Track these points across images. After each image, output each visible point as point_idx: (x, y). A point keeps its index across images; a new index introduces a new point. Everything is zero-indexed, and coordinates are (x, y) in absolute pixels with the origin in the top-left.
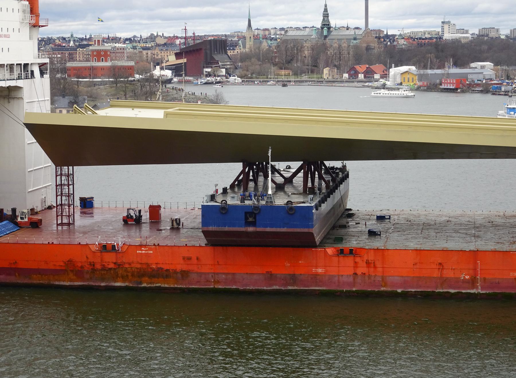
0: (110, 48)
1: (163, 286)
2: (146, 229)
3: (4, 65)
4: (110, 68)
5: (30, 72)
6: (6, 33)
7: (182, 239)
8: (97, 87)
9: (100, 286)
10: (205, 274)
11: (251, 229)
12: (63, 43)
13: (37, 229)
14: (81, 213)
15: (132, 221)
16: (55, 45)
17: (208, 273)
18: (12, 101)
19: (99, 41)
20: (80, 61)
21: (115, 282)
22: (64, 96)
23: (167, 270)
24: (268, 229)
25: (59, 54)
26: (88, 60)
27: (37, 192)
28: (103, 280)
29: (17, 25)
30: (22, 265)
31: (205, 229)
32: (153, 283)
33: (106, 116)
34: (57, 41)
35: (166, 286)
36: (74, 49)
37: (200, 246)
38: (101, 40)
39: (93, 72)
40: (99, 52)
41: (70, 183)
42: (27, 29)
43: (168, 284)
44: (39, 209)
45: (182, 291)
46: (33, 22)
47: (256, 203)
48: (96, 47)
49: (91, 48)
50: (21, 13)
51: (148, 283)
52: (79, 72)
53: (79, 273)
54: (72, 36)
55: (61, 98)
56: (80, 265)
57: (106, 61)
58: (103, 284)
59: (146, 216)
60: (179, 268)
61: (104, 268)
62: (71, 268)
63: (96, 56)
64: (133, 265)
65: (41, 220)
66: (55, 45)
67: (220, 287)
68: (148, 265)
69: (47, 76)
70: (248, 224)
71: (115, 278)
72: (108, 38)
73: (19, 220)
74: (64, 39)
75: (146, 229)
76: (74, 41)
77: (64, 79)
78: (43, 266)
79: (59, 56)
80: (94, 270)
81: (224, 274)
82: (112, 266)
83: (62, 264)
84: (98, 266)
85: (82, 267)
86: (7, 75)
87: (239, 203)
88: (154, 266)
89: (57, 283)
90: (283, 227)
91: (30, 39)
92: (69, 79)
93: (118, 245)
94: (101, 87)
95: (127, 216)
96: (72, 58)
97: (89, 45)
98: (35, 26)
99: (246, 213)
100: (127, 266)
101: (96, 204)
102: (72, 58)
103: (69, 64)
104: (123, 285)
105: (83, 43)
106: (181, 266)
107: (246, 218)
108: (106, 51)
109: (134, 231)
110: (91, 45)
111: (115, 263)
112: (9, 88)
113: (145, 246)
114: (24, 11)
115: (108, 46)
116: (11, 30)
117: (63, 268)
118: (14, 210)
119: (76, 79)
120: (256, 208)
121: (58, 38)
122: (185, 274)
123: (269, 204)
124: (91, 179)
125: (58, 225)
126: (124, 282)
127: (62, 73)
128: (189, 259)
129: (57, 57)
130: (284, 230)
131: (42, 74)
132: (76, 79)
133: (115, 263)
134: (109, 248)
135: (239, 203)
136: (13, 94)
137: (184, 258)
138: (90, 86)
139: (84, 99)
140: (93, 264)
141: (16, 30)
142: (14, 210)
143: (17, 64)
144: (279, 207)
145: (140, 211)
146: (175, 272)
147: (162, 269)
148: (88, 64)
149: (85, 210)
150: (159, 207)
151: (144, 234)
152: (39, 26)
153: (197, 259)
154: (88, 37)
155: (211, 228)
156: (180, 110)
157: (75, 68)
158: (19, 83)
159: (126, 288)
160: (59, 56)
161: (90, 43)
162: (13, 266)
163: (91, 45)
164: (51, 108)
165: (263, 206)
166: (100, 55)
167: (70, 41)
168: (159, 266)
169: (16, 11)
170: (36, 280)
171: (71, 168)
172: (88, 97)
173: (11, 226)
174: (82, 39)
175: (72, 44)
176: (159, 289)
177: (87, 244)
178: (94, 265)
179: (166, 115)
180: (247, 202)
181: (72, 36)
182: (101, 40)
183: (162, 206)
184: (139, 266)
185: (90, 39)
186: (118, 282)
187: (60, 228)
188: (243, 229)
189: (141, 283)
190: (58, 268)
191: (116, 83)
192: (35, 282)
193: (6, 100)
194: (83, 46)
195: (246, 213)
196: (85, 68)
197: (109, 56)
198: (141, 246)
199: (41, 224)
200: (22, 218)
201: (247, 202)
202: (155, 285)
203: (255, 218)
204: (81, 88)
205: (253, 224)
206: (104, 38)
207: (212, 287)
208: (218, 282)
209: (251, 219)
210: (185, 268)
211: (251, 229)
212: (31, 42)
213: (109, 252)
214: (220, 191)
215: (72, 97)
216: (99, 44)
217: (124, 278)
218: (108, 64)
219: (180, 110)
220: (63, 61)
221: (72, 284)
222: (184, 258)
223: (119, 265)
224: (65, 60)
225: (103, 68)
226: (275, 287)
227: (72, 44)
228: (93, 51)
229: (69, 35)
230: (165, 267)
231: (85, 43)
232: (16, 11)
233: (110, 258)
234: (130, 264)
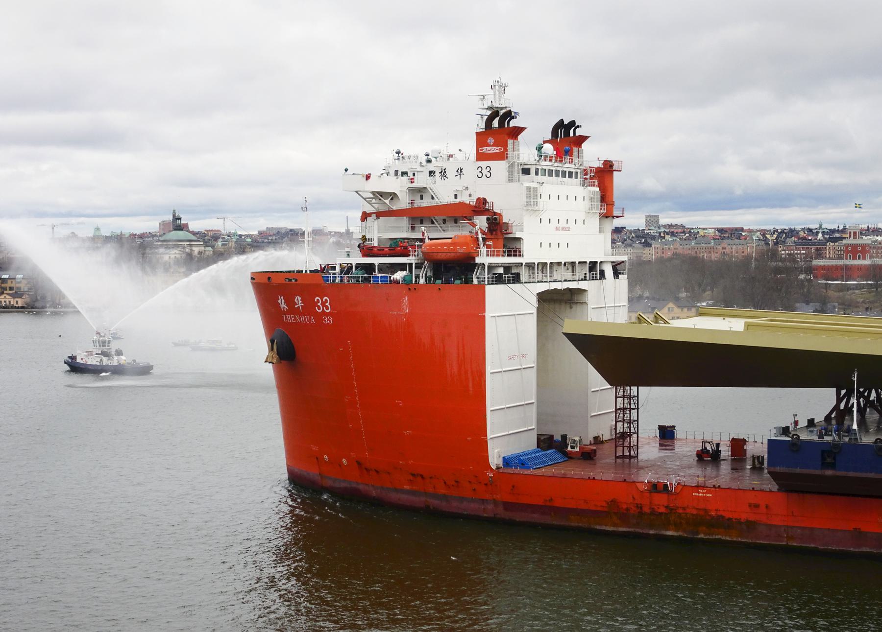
0: (870, 242)
1: (724, 538)
2: (725, 467)
3: (585, 262)
4: (867, 268)
5: (598, 272)
6: (565, 225)
7: (748, 480)
8: (850, 292)
9: (649, 534)
10: (775, 526)
11: (829, 472)
12: (808, 235)
13: (591, 462)
14: (661, 445)
15: (708, 456)
16: (799, 238)
17: (780, 526)
18: (574, 307)
19: (855, 233)
20: (830, 258)
21: (667, 530)
22: (807, 303)
23: (729, 519)
24: (851, 474)
25: (803, 249)
26: (840, 258)
27: (606, 416)
28: (651, 527)
29: (581, 216)
30: (558, 503)
31: (772, 469)
32: (712, 534)
33: (730, 331)
34: (802, 233)
35: (728, 539)
36: (823, 243)
37: (771, 491)
38: (858, 231)
39: (846, 272)
40: (854, 246)
41: (633, 406)
42: (596, 220)
43: (730, 536)
44: (605, 438)
45: (747, 546)
46: (604, 211)
47: (836, 438)
48: (851, 241)
49: (844, 242)
50: (587, 201)
51: (705, 534)
52: (830, 273)
53: (624, 517)
54: (821, 226)
55: (804, 304)
56: (625, 506)
57: (864, 258)
58: (652, 532)
59: (726, 452)
60: (744, 517)
61: (653, 512)
62: (614, 510)
63: (850, 252)
64: (688, 511)
65: (595, 450)
66: (799, 238)
67: (795, 544)
68: (705, 510)
69: (623, 279)
70: (825, 465)
71: (667, 526)
72: (868, 229)
73: (569, 449)
74: (810, 230)
75: (725, 467)
76: (823, 233)
77: (810, 281)
78: (584, 506)
79: (803, 252)
80: (641, 514)
81: (800, 528)
82: (662, 510)
83: (604, 504)
84: (646, 510)
85: (627, 509)
86: (569, 276)
87: (816, 438)
88: (713, 513)
89: (598, 527)
90: (871, 472)
91: (600, 232)
92: (815, 281)
93: (671, 484)
94: (857, 291)
95: (702, 450)
96: (819, 255)
97: (842, 238)
98: (607, 215)
99: (823, 452)
100: (680, 511)
101: (678, 434)
102: (820, 255)
103: (816, 263)
104: (675, 534)
105: (834, 236)
106: (745, 515)
107: (823, 458)
108: (864, 246)
109: (710, 471)
110: (845, 238)
111: (666, 507)
112: (569, 290)
113: (703, 487)
114: (591, 199)
115: (867, 240)
116: (571, 223)
117: (606, 509)
118: (564, 437)
119: (823, 282)
120: (834, 445)
121: (803, 229)
122: (751, 525)
123: (853, 442)
124: (658, 403)
125: (616, 457)
126: (676, 530)
127: (806, 273)
128: (757, 506)
129: (800, 254)
130: (872, 475)
131: (616, 274)
132: (823, 282)
133: (666, 507)
134: (661, 488)
135: (816, 438)
136: (575, 298)
137: (750, 505)
138: (841, 291)
139: (834, 307)
140: (640, 507)
141: (580, 222)
142: (564, 437)
143: (580, 263)
144: (866, 446)
145: (718, 445)
146: (739, 522)
147: (723, 517)
148: (840, 262)
149: (665, 442)
150: (744, 441)
151: (724, 474)
152: (613, 217)
153: (767, 507)
154: (841, 228)
155: (779, 469)
156: (772, 320)
157: (823, 268)
158: (582, 285)
159: (679, 538)
160: (803, 252)
161: (844, 236)
162: (548, 504)
163: (845, 238)
164: (484, 312)
165: (845, 444)
166: (855, 251)
167: (817, 233)
168: (719, 513)
169: (580, 199)
170: (574, 522)
171: (634, 388)
172: (839, 304)
173: (558, 457)
174: (833, 231)
175: (820, 237)
176: (720, 541)
177: (634, 482)
178: (641, 508)
179: (748, 326)
180: (828, 439)
181: (821, 226)
182: (858, 231)
183: (751, 440)
184: (695, 512)
185: (844, 230)
186: (669, 530)
187: (619, 461)
188: (818, 472)
189: (698, 533)
190: (599, 509)
191: (876, 286)
192: (573, 524)
193: (568, 306)
194: (835, 240)
195: (823, 452)
196: (837, 268)
197: (868, 252)
198: (698, 487)
199: (595, 455)
200: (572, 447)
201: (828, 439)
202: (714, 537)
203: (834, 459)
204: (831, 293)
205: (832, 466)
206: (862, 230)
207: (784, 543)
208: (790, 538)
209: (829, 460)
210: (752, 518)
211: (829, 472)
212: (602, 236)
213: (659, 492)
214: (803, 423)
215: (818, 304)
216: (855, 237)
217: (677, 527)
218: (867, 262)
219: (772, 320)
220: (808, 258)
221: (615, 529)
222: (750, 505)
223: (671, 510)
224: (811, 258)
225: (859, 268)
226: (864, 549)
227: (820, 237)
228: (847, 246)
229: (817, 226)
230: (727, 515)
231: (837, 235)
232: (580, 199)
233: (660, 500)
234: (684, 509)
